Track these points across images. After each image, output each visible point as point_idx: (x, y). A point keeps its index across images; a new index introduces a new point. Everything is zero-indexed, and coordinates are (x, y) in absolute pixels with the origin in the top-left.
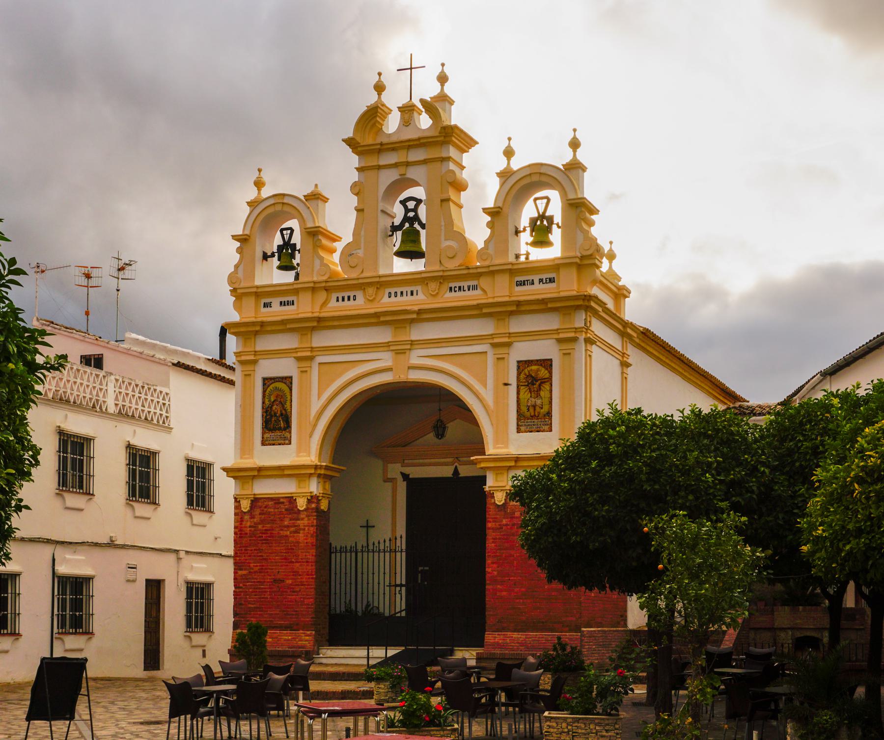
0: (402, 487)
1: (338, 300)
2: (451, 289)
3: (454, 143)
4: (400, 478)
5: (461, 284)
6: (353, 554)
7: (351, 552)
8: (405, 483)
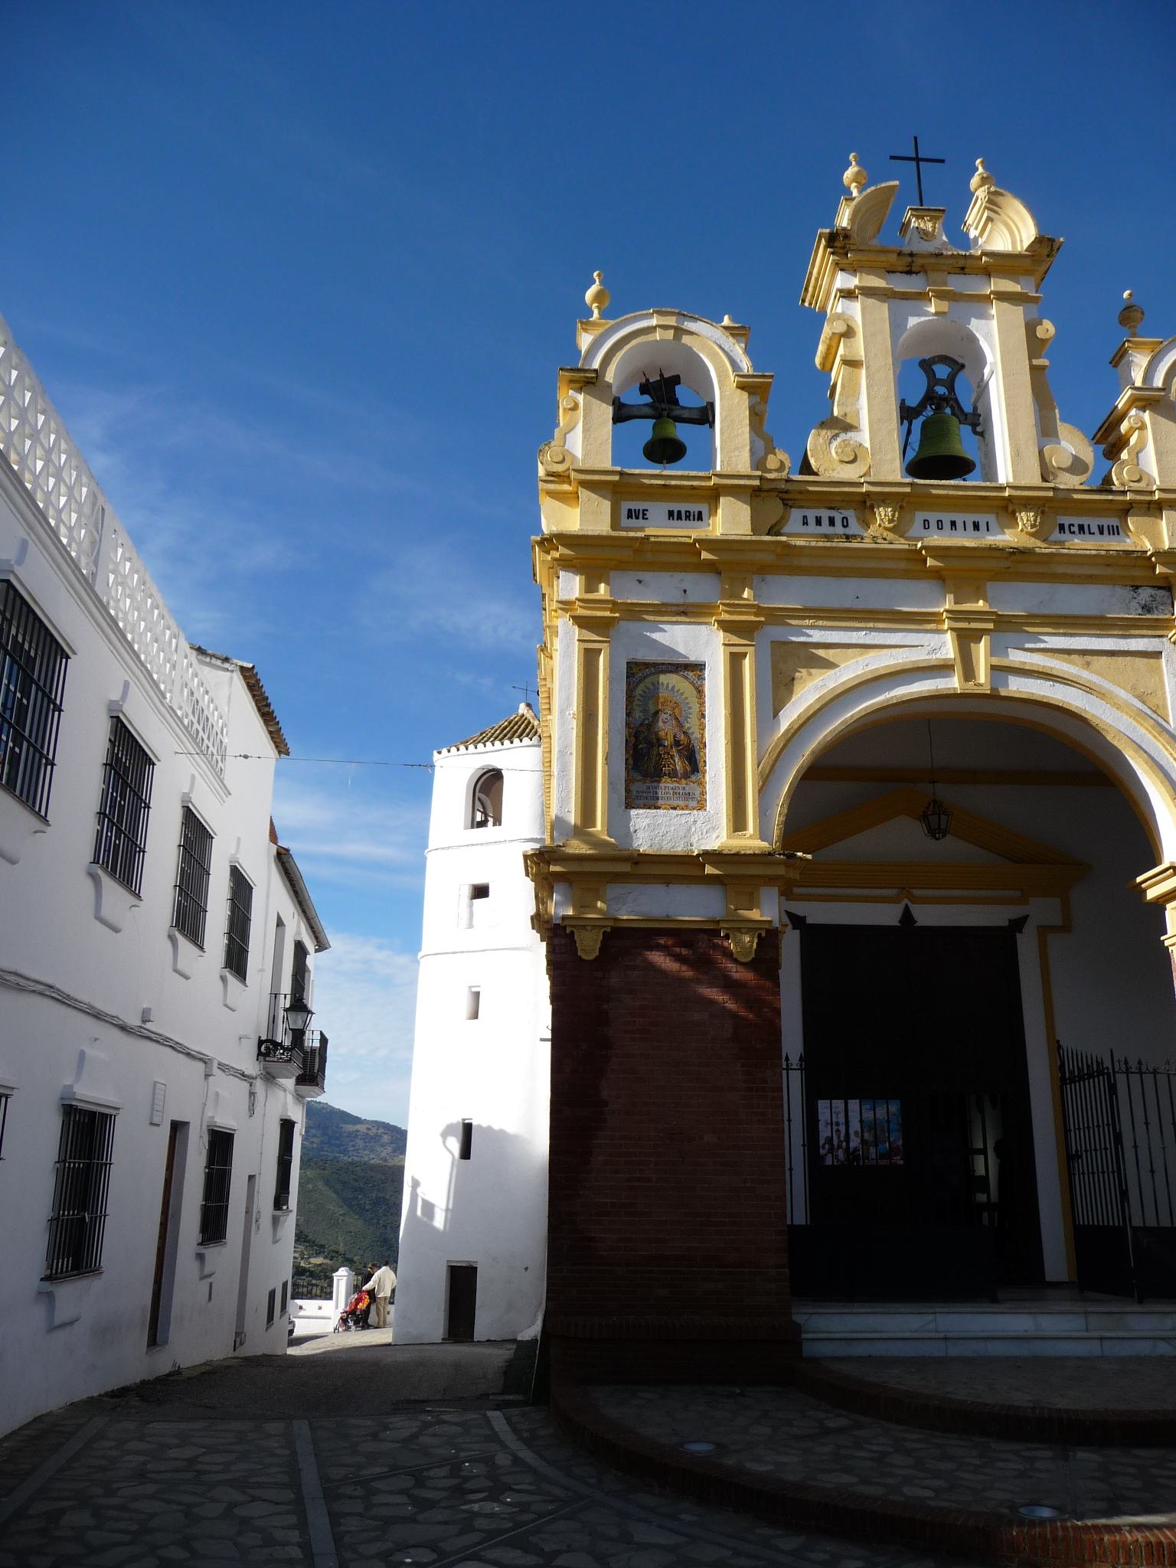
1: (805, 523)
5: (1085, 521)
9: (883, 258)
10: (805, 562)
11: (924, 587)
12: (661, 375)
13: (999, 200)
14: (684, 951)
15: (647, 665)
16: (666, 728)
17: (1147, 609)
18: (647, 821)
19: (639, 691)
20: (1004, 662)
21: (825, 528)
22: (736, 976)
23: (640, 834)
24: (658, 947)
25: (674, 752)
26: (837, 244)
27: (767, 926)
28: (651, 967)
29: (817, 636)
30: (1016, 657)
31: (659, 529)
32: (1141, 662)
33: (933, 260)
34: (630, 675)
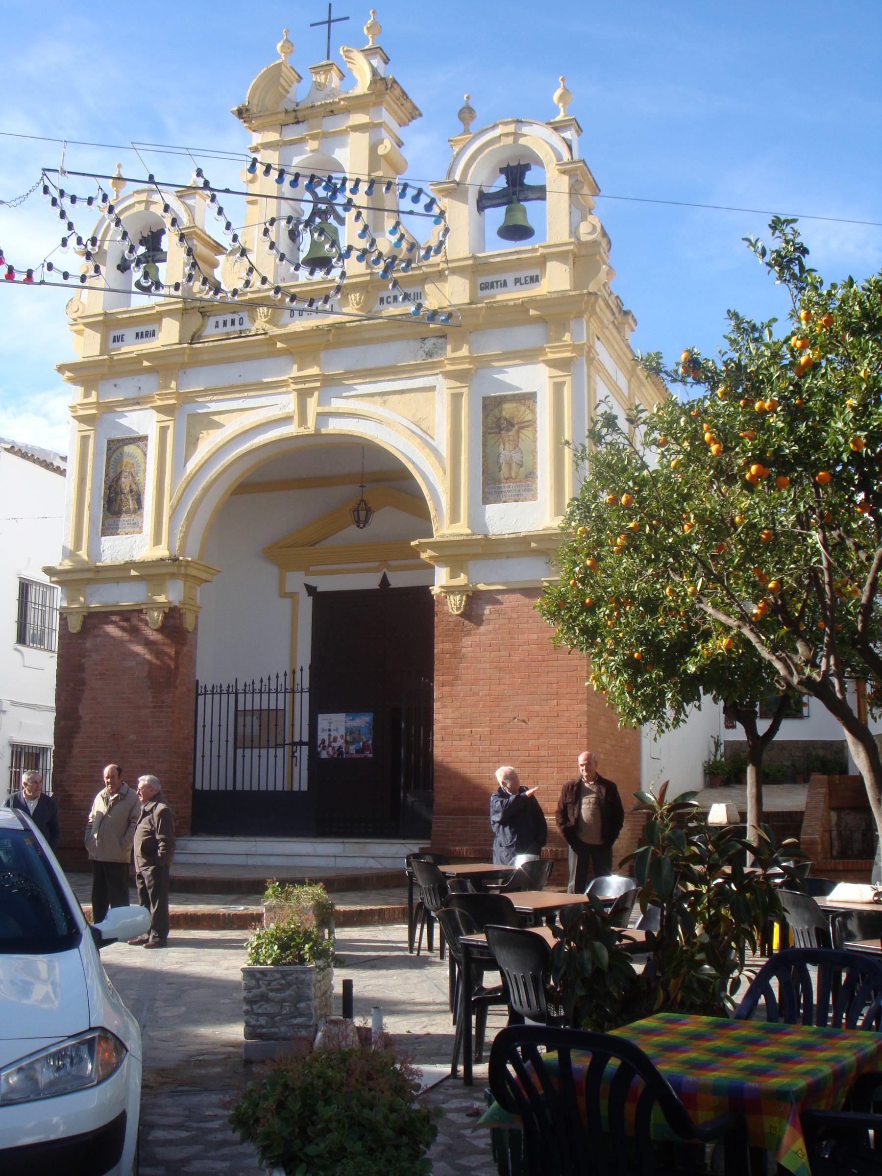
0: (306, 604)
1: (217, 326)
2: (382, 300)
3: (388, 104)
4: (304, 592)
6: (232, 696)
7: (228, 693)
8: (311, 598)
9: (274, 118)
10: (206, 357)
11: (282, 361)
12: (151, 231)
13: (351, 55)
14: (125, 624)
15: (118, 441)
16: (126, 483)
17: (429, 354)
18: (110, 544)
19: (113, 459)
20: (326, 409)
21: (229, 328)
22: (152, 638)
23: (106, 552)
24: (112, 622)
25: (129, 497)
26: (244, 115)
27: (168, 605)
28: (107, 635)
29: (214, 407)
30: (337, 404)
31: (132, 348)
32: (420, 395)
33: (309, 112)
34: (485, 407)
